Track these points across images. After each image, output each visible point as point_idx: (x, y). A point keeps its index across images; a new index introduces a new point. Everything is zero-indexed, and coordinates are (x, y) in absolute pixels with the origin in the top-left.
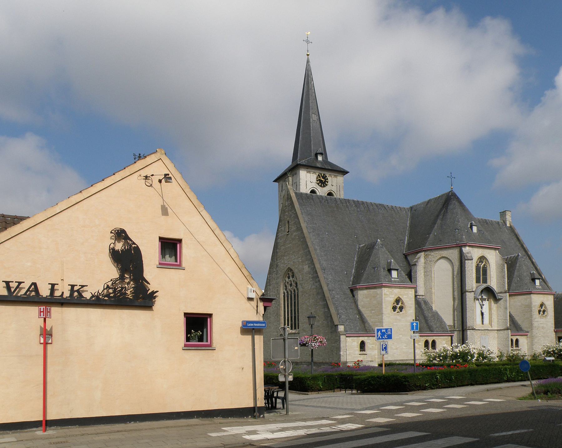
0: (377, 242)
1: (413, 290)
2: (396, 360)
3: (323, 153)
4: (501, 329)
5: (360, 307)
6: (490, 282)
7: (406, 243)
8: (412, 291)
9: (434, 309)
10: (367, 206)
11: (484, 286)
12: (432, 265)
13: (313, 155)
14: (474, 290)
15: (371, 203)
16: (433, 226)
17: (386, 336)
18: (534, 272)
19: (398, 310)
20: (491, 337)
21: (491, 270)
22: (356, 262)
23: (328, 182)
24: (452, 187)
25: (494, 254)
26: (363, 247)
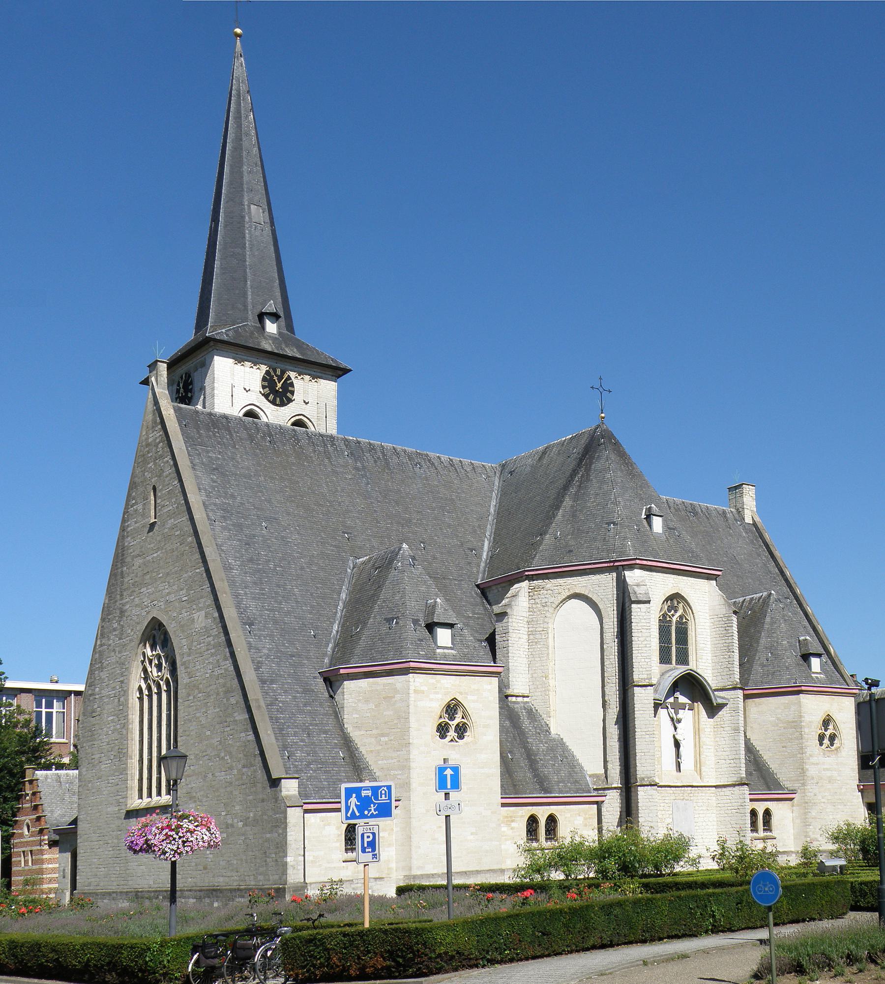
0: (400, 550)
1: (495, 681)
3: (282, 314)
4: (726, 783)
5: (349, 728)
8: (490, 684)
9: (553, 731)
10: (384, 455)
11: (679, 670)
13: (250, 317)
14: (654, 681)
16: (553, 513)
17: (372, 809)
18: (808, 638)
19: (452, 734)
20: (699, 804)
21: (698, 630)
23: (292, 393)
24: (603, 415)
25: (707, 589)
26: (364, 563)
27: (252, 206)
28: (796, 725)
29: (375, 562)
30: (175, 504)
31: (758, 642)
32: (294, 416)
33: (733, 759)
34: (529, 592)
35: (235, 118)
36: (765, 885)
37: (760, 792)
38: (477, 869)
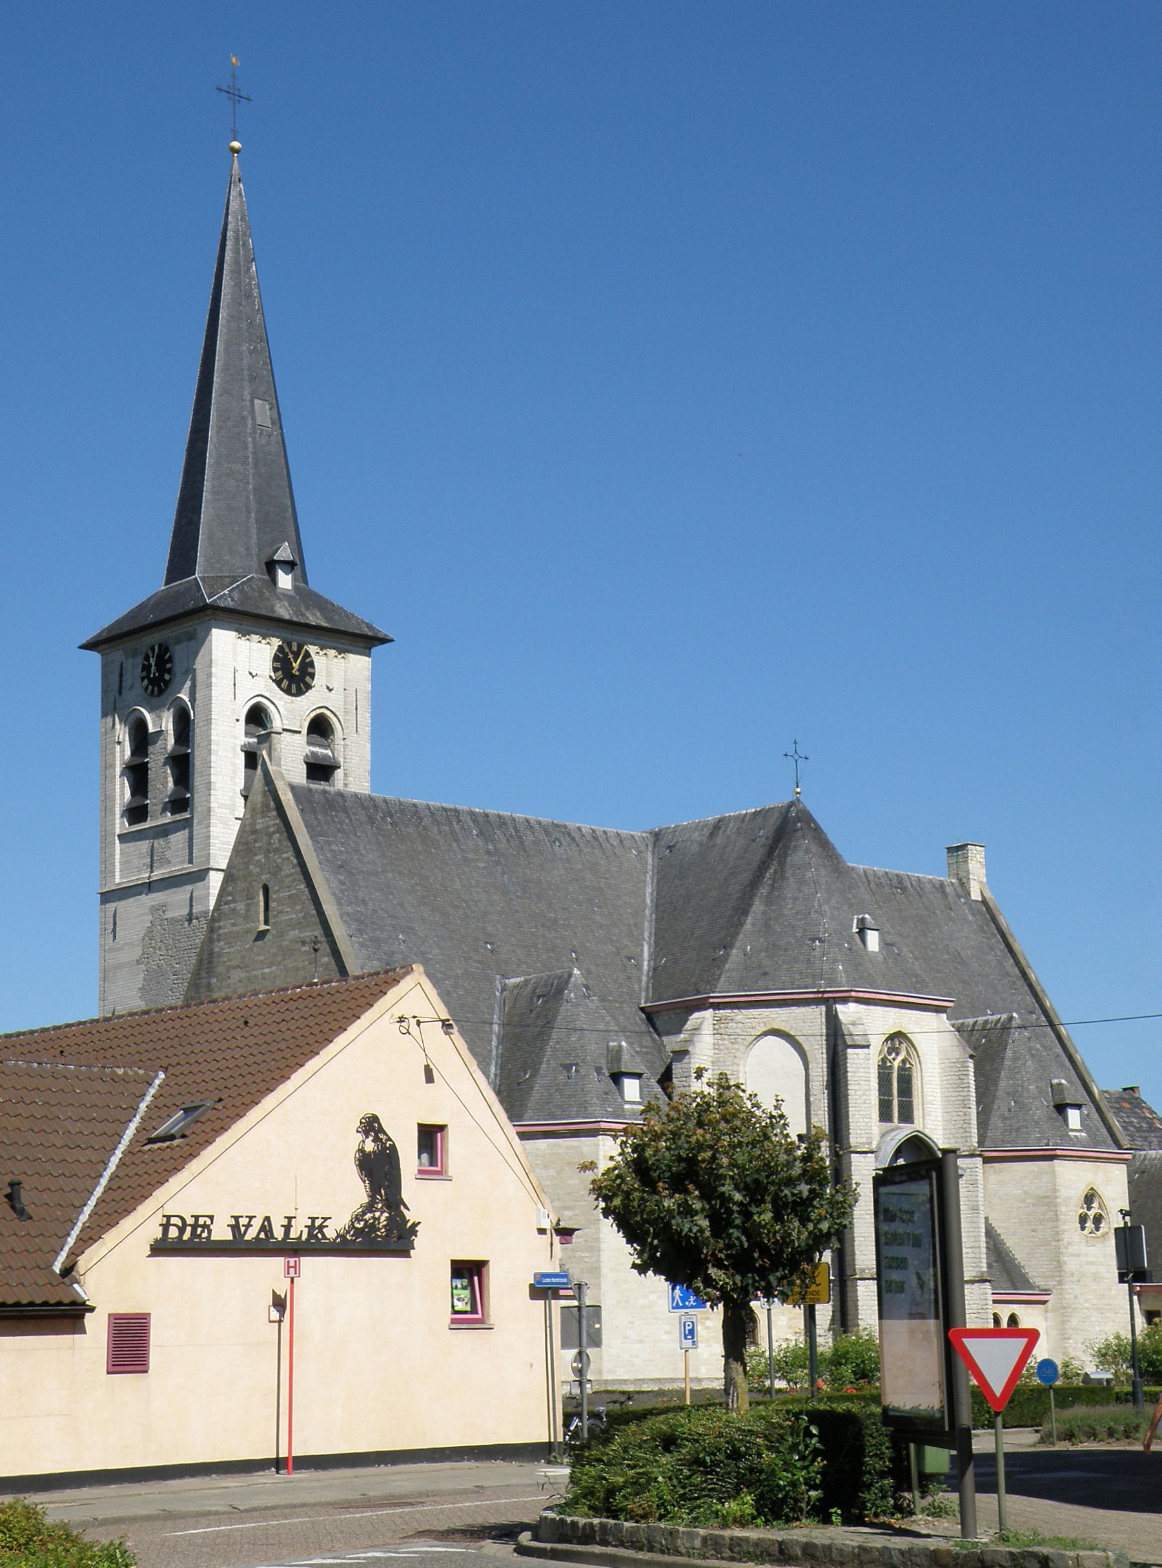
2: (639, 1380)
6: (924, 1118)
7: (646, 967)
10: (517, 831)
12: (738, 1054)
14: (874, 1146)
15: (527, 821)
18: (1063, 1081)
21: (925, 1079)
22: (498, 1039)
23: (312, 676)
24: (798, 790)
26: (517, 986)
27: (257, 402)
28: (1049, 1201)
29: (536, 988)
30: (300, 913)
31: (996, 1085)
32: (315, 710)
33: (971, 1248)
34: (714, 1024)
35: (232, 272)
36: (1047, 1370)
37: (1003, 1292)
38: (672, 1376)
